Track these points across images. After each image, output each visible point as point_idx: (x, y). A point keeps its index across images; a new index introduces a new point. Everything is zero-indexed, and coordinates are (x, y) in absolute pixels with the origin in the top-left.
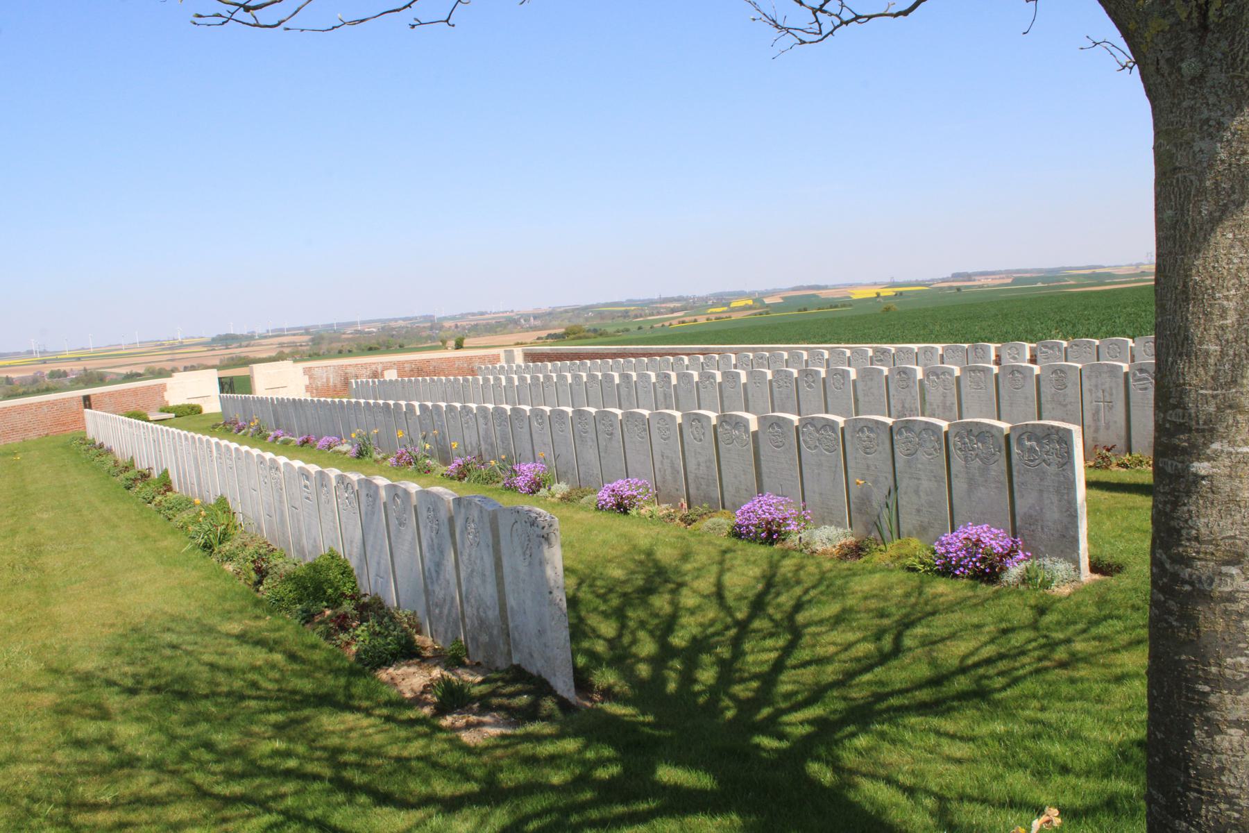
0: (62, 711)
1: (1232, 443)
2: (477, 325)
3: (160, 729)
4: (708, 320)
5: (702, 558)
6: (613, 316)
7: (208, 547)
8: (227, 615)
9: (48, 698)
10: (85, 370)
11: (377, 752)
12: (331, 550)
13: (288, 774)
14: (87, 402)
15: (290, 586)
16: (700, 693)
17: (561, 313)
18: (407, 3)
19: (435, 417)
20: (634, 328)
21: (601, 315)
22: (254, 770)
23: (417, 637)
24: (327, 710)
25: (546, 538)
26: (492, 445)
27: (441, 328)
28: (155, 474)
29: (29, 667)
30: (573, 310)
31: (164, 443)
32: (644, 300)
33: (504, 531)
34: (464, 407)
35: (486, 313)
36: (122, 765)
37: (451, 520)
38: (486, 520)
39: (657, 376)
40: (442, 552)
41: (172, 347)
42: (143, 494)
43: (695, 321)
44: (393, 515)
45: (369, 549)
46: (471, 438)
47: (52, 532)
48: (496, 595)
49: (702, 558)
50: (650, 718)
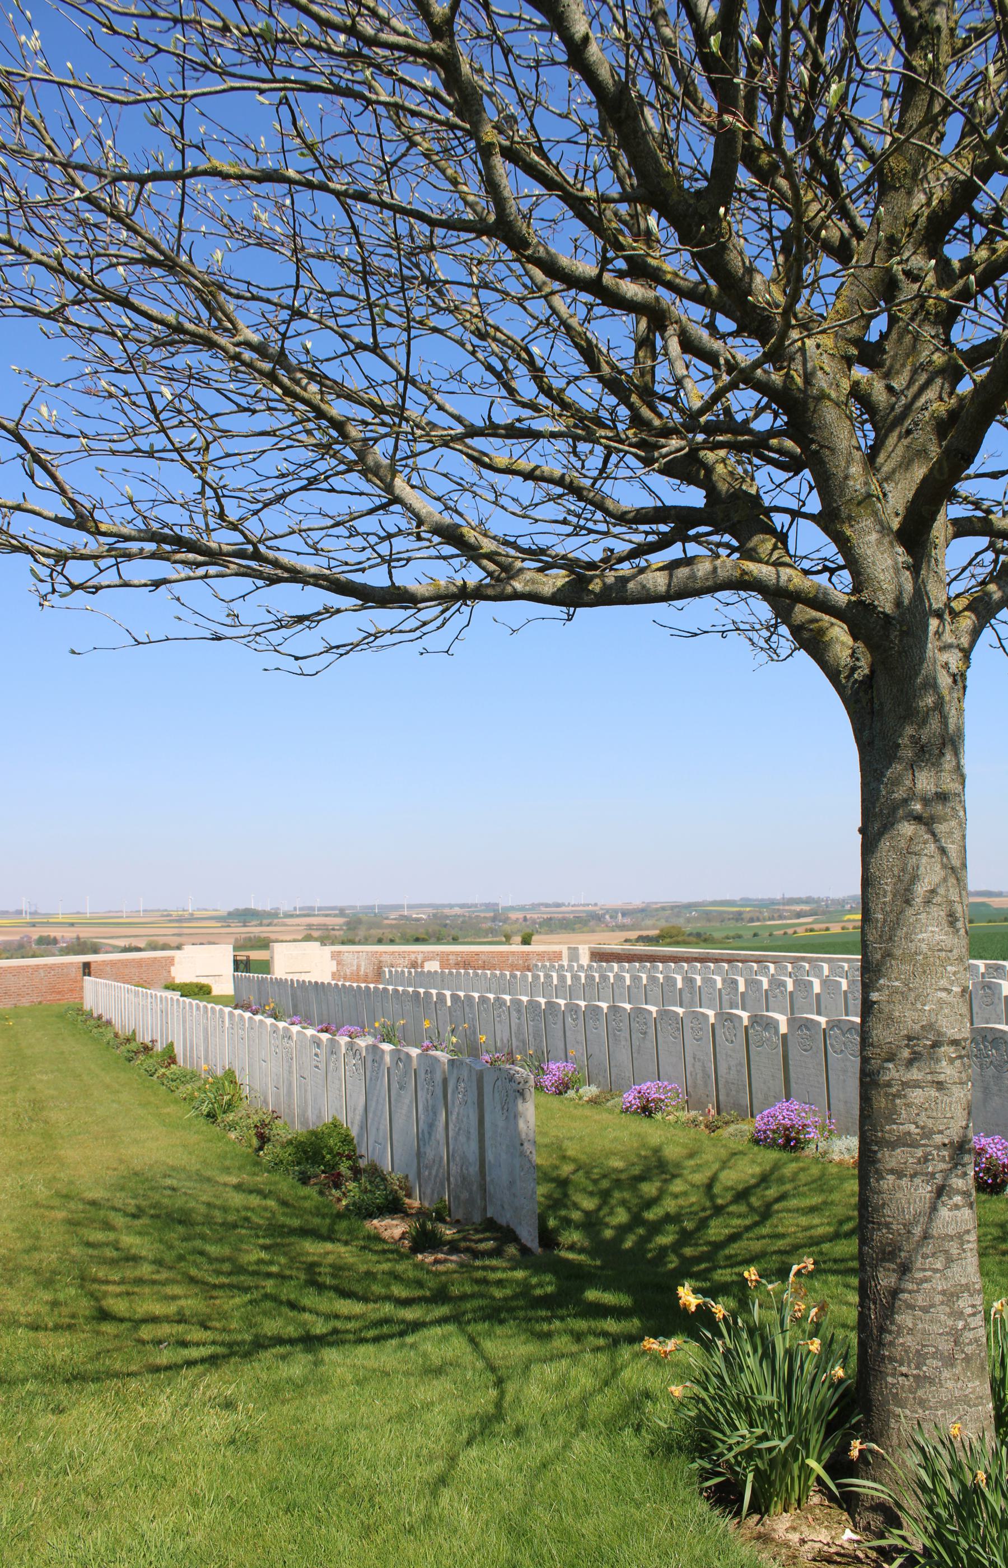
0: (72, 1223)
1: (889, 979)
2: (551, 919)
3: (161, 1241)
4: (843, 928)
5: (708, 1157)
6: (721, 917)
7: (211, 1116)
8: (227, 1170)
9: (61, 1215)
10: (78, 938)
11: (349, 1268)
12: (334, 1118)
13: (269, 1275)
14: (87, 968)
15: (290, 1149)
16: (650, 1251)
17: (657, 910)
18: (873, 16)
19: (467, 1009)
20: (748, 934)
21: (708, 916)
22: (240, 1270)
23: (407, 1201)
24: (309, 1239)
25: (521, 1093)
26: (523, 1042)
27: (506, 920)
28: (159, 1048)
29: (41, 1192)
30: (672, 908)
31: (172, 1014)
32: (762, 900)
33: (487, 1089)
34: (497, 999)
35: (563, 905)
36: (127, 1259)
37: (445, 1081)
38: (474, 1078)
39: (724, 981)
40: (435, 1113)
41: (180, 920)
42: (145, 1066)
43: (827, 929)
44: (395, 1079)
45: (370, 1115)
46: (502, 1034)
47: (52, 1092)
48: (477, 1151)
49: (708, 1157)
50: (598, 1263)
